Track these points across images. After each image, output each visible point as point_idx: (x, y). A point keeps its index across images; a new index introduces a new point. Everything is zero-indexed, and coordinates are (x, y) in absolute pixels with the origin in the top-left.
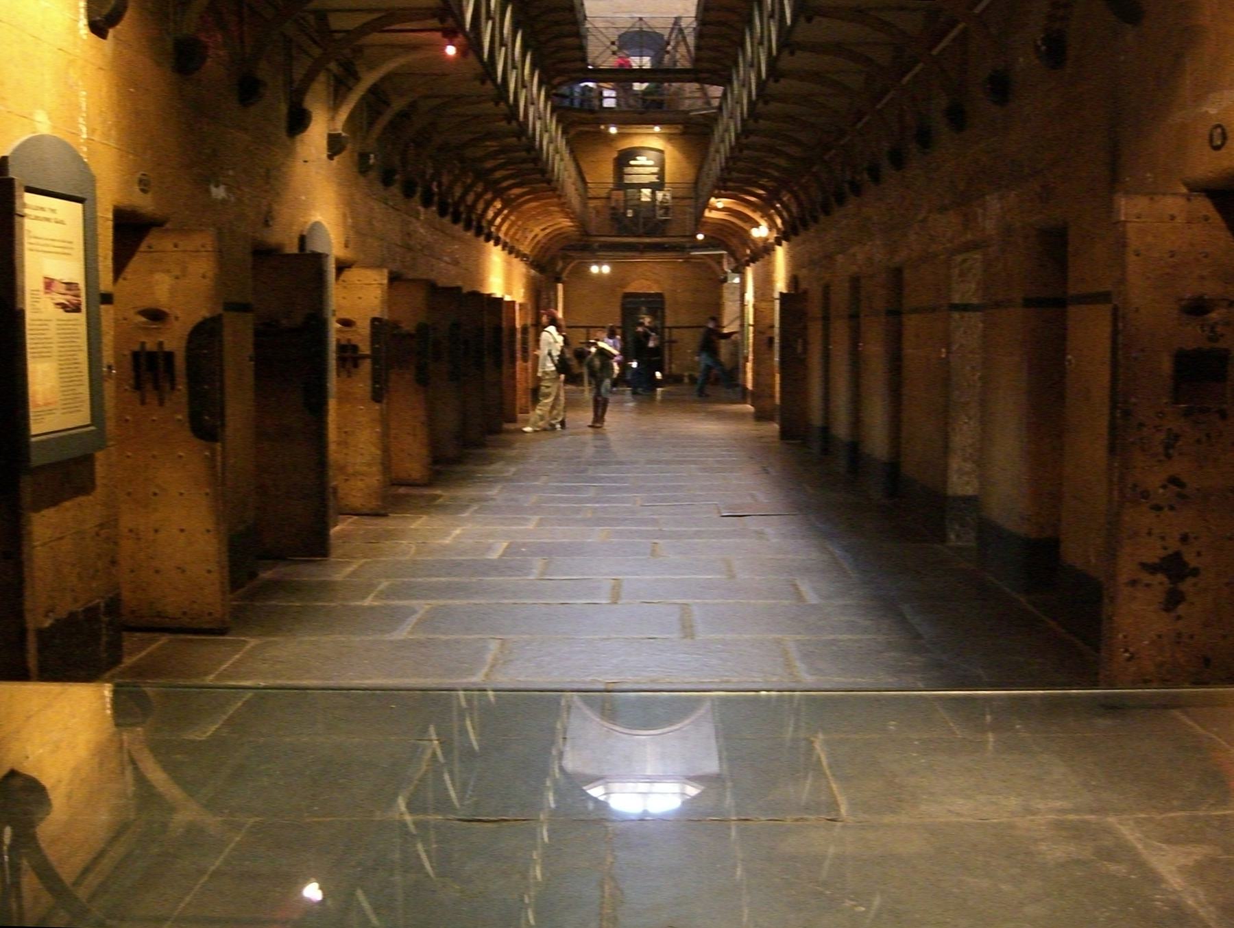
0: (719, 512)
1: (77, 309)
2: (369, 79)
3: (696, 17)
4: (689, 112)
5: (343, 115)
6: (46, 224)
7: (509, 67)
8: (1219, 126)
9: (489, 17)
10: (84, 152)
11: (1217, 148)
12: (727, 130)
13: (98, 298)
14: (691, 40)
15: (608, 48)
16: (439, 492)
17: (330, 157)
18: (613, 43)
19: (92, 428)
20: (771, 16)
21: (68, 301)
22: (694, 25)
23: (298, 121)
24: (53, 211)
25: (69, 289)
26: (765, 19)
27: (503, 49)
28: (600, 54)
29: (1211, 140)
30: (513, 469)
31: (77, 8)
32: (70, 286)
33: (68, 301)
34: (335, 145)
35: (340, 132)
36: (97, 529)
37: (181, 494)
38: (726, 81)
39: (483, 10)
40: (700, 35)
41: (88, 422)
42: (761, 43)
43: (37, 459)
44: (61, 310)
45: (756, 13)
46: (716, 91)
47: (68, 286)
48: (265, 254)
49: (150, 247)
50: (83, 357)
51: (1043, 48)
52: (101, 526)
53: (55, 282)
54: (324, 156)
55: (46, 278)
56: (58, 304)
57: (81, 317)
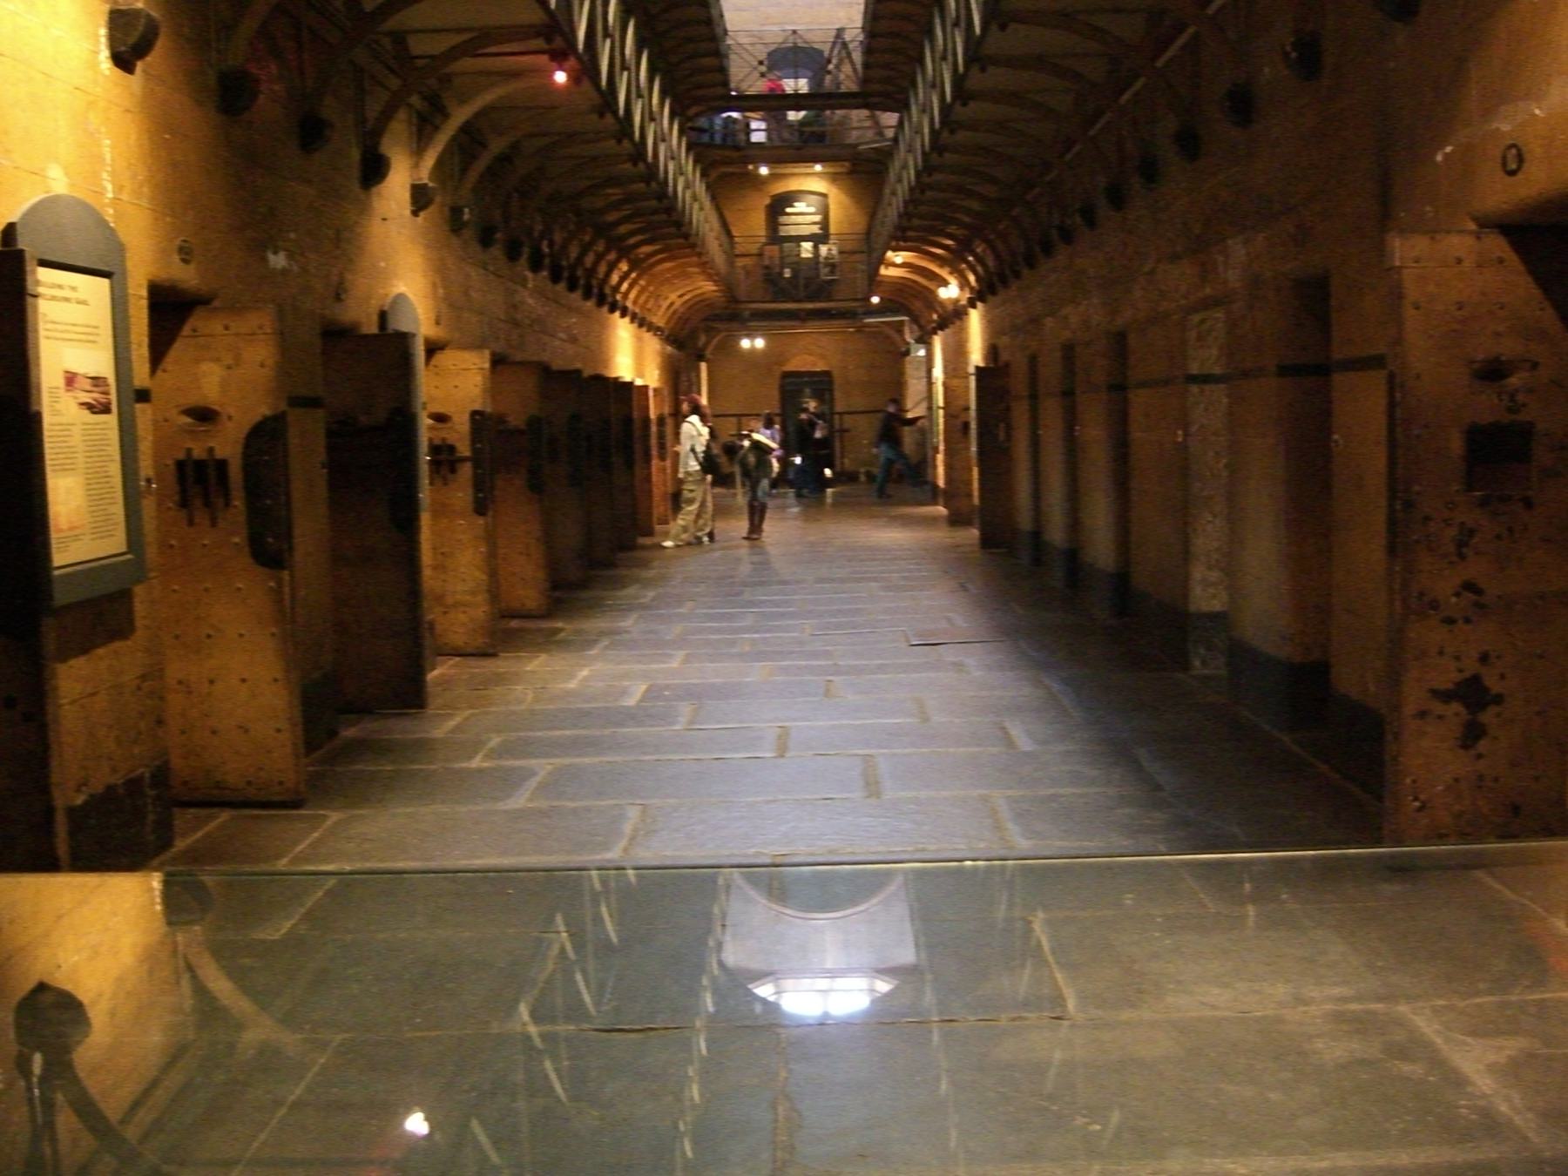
0: (908, 641)
1: (106, 410)
2: (460, 115)
3: (863, 28)
5: (429, 160)
7: (634, 95)
8: (1514, 146)
9: (607, 34)
11: (1512, 173)
12: (905, 167)
14: (857, 57)
15: (755, 68)
16: (560, 625)
17: (415, 213)
18: (761, 63)
19: (129, 556)
20: (956, 24)
21: (95, 400)
23: (374, 170)
24: (74, 289)
26: (949, 29)
28: (746, 77)
29: (1504, 158)
30: (651, 594)
31: (97, 36)
32: (97, 381)
33: (95, 400)
34: (420, 198)
38: (902, 106)
40: (868, 50)
41: (124, 549)
46: (890, 119)
47: (95, 382)
48: (337, 335)
50: (115, 469)
52: (143, 677)
53: (79, 376)
54: (407, 212)
56: (82, 404)
57: (111, 420)
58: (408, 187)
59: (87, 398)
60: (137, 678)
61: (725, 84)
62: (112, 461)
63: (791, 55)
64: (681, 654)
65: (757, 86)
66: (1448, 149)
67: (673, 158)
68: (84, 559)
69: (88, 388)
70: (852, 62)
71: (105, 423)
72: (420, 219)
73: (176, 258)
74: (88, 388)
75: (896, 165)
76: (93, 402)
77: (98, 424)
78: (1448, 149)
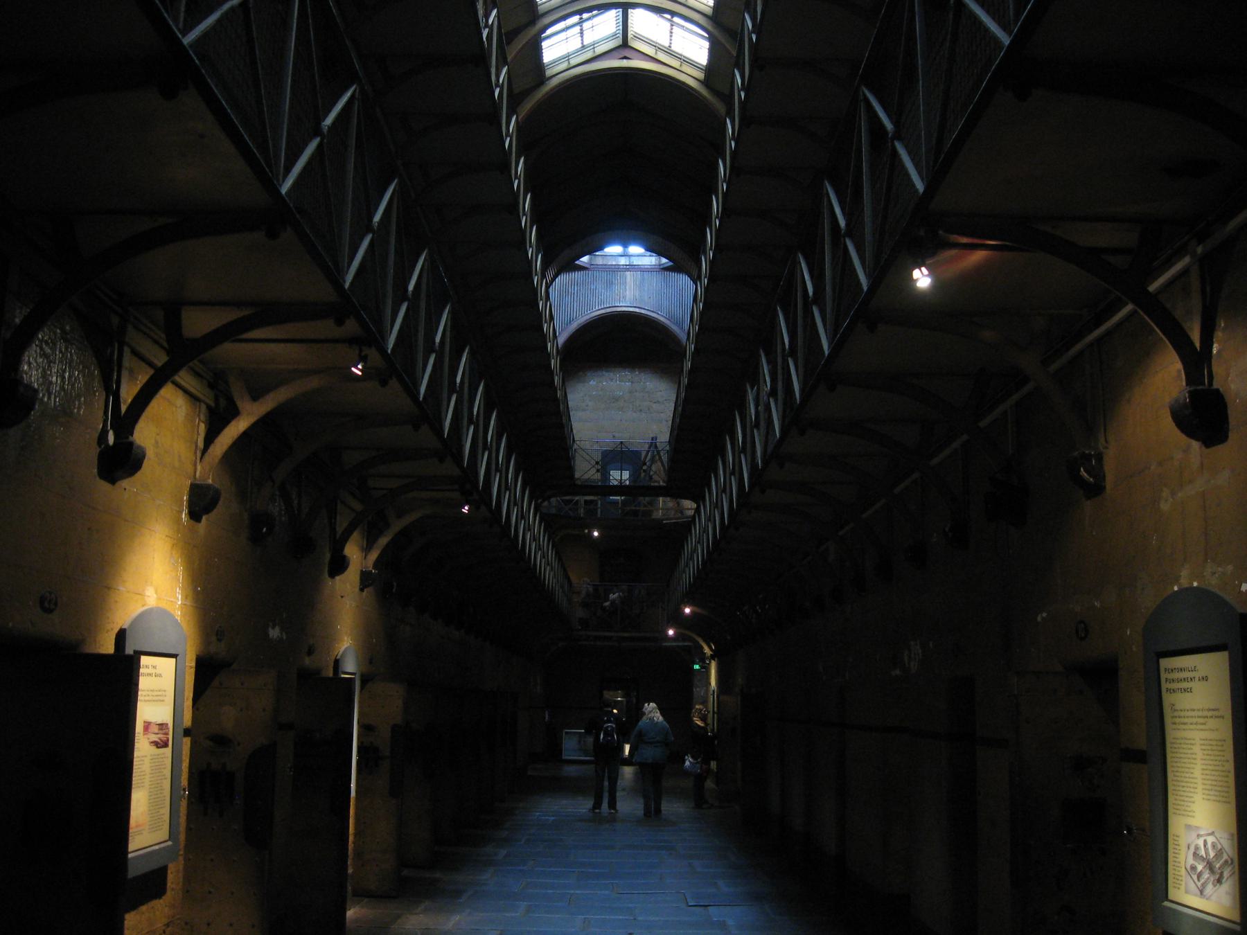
0: (687, 903)
1: (165, 745)
2: (397, 526)
3: (669, 442)
4: (662, 520)
5: (374, 556)
6: (149, 678)
7: (512, 504)
8: (1082, 622)
9: (497, 470)
10: (178, 616)
11: (1082, 639)
12: (695, 551)
13: (182, 732)
14: (665, 458)
15: (593, 466)
16: (438, 875)
17: (362, 590)
18: (597, 463)
19: (170, 843)
20: (733, 473)
21: (160, 739)
22: (668, 448)
23: (339, 565)
24: (154, 667)
25: (161, 729)
26: (728, 475)
27: (508, 493)
28: (585, 470)
29: (1077, 632)
30: (503, 852)
31: (182, 500)
32: (162, 726)
33: (160, 739)
34: (366, 579)
35: (371, 569)
36: (164, 928)
37: (232, 893)
38: (698, 498)
39: (493, 467)
40: (672, 460)
41: (167, 838)
42: (724, 491)
43: (132, 872)
44: (155, 747)
45: (720, 462)
46: (689, 505)
47: (161, 727)
48: (309, 677)
49: (221, 684)
50: (167, 785)
51: (950, 534)
52: (167, 925)
53: (152, 724)
54: (357, 590)
55: (144, 722)
56: (152, 742)
57: (168, 751)
58: (359, 572)
59: (154, 738)
60: (165, 925)
61: (572, 477)
62: (165, 779)
63: (618, 456)
64: (524, 905)
65: (593, 475)
66: (1044, 615)
67: (534, 540)
68: (140, 847)
69: (156, 731)
70: (662, 462)
71: (163, 754)
72: (365, 593)
73: (214, 638)
74: (156, 731)
75: (692, 540)
76: (159, 741)
77: (158, 755)
78: (1044, 615)
